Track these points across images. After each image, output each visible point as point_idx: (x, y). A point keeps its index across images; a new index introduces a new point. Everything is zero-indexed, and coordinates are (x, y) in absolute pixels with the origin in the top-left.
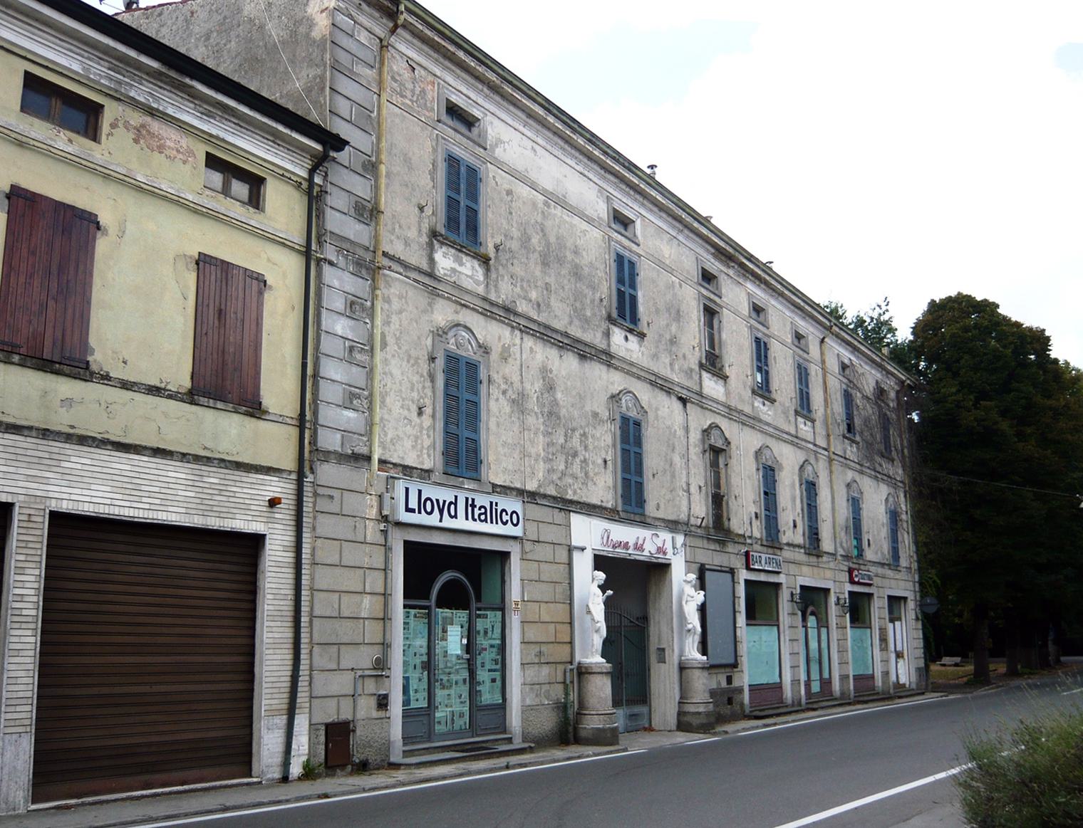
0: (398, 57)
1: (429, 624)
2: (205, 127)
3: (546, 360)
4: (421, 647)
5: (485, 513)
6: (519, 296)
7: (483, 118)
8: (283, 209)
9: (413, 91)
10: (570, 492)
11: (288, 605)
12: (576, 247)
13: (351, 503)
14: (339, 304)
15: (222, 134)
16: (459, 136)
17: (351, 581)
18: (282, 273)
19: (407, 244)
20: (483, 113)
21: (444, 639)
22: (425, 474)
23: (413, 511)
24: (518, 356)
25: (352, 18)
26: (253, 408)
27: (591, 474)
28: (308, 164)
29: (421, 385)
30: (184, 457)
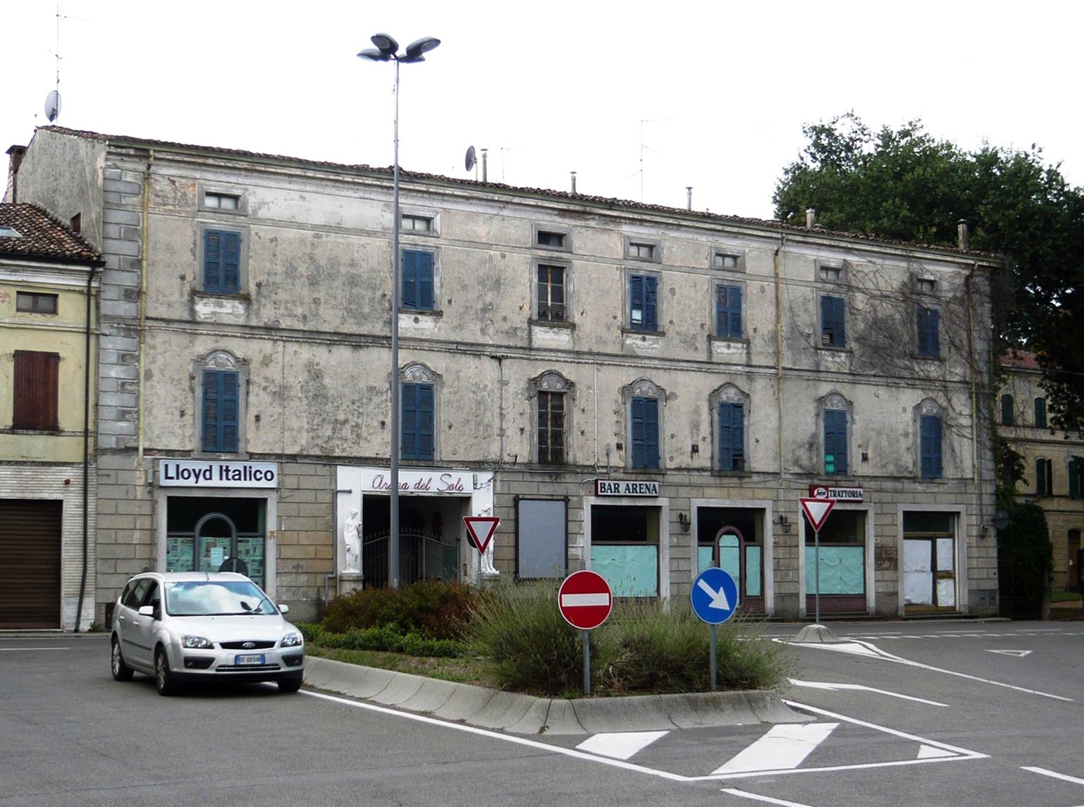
0: (160, 179)
1: (194, 546)
2: (14, 278)
3: (312, 357)
4: (187, 561)
5: (239, 474)
6: (283, 315)
7: (244, 194)
8: (71, 310)
9: (175, 198)
10: (337, 450)
11: (79, 538)
12: (352, 260)
13: (123, 477)
14: (114, 359)
15: (25, 279)
16: (218, 215)
17: (126, 522)
18: (70, 350)
19: (170, 305)
20: (242, 189)
21: (208, 556)
22: (186, 454)
23: (172, 478)
24: (280, 359)
25: (117, 168)
26: (53, 428)
27: (364, 434)
28: (86, 278)
29: (183, 397)
30: (9, 463)
